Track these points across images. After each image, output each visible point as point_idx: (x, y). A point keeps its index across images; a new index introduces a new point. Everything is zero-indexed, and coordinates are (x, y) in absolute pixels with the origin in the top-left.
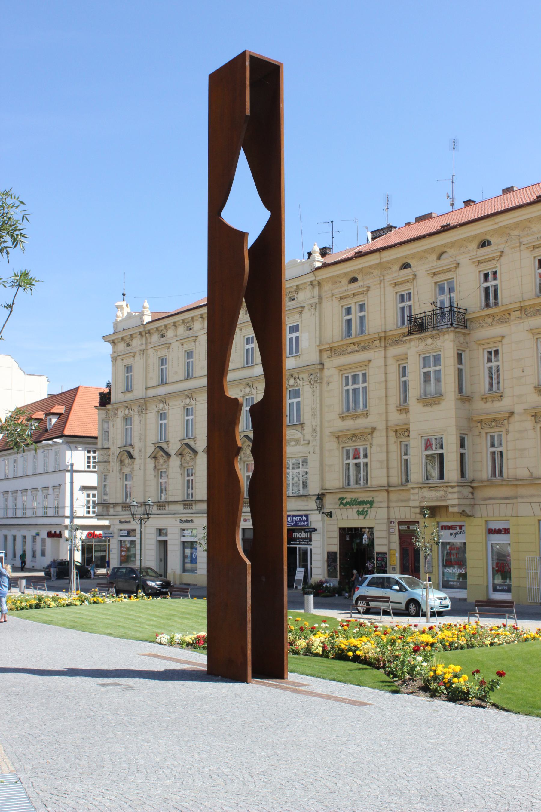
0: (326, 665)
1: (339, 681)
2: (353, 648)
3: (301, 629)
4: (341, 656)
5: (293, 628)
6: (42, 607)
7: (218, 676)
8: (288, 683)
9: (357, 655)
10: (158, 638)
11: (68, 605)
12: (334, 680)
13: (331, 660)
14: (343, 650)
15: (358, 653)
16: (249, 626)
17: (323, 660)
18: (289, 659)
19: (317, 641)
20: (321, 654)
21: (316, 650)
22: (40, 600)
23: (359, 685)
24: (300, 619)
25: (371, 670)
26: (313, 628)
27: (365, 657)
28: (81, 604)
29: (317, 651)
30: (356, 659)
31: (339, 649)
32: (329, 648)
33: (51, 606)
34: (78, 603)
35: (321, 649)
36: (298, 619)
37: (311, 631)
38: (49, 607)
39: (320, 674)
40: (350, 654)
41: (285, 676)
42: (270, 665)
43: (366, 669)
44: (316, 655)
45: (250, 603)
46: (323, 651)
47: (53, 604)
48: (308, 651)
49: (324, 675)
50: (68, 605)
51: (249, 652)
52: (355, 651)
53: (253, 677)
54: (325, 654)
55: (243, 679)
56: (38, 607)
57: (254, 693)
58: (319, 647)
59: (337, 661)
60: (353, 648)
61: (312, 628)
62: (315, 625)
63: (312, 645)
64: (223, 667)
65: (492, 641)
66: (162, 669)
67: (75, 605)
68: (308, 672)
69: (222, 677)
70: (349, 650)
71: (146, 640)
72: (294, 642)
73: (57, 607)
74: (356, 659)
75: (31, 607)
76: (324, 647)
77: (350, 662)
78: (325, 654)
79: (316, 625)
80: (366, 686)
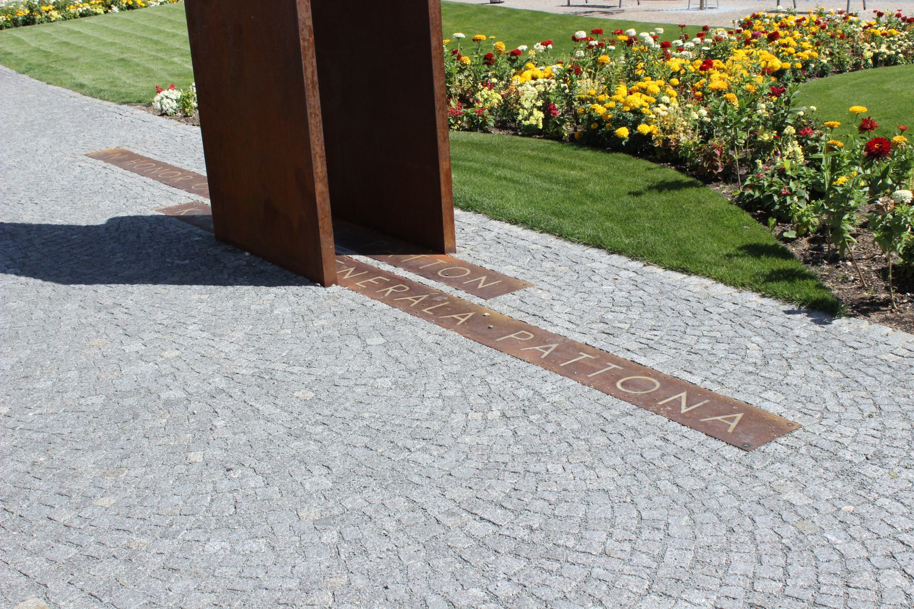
0: (561, 172)
1: (614, 251)
2: (631, 116)
3: (488, 60)
4: (596, 136)
5: (468, 62)
6: (37, 21)
7: (245, 249)
8: (453, 276)
9: (640, 135)
10: (158, 97)
11: (82, 15)
12: (599, 247)
13: (568, 150)
14: (601, 121)
15: (644, 129)
16: (313, 101)
17: (546, 150)
18: (455, 151)
19: (530, 86)
20: (541, 126)
21: (526, 119)
22: (31, 9)
23: (684, 271)
24: (483, 37)
25: (692, 191)
26: (516, 53)
27: (666, 141)
28: (106, 12)
29: (532, 121)
30: (640, 146)
31: (590, 116)
32: (559, 108)
33: (53, 19)
34: (100, 10)
35: (540, 115)
36: (478, 36)
37: (509, 59)
38: (49, 19)
39: (555, 221)
40: (623, 132)
41: (447, 244)
42: (389, 207)
43: (677, 185)
44: (531, 131)
45: (310, 23)
46: (545, 121)
47: (55, 14)
48: (507, 116)
49: (567, 225)
50: (82, 15)
51: (321, 188)
52: (636, 124)
53: (350, 242)
54: (550, 131)
55: (309, 272)
56: (29, 21)
57: (333, 329)
58: (535, 111)
59: (588, 153)
60: (631, 116)
61: (513, 54)
62: (520, 48)
63: (517, 101)
64: (249, 232)
65: (877, 51)
66: (95, 214)
67: (96, 14)
68: (514, 211)
69: (252, 253)
70: (619, 122)
71: (140, 102)
72: (473, 94)
73: (65, 19)
74: (640, 146)
75: (15, 23)
76: (547, 108)
77: (621, 155)
78: (550, 131)
79: (523, 47)
80: (709, 277)
